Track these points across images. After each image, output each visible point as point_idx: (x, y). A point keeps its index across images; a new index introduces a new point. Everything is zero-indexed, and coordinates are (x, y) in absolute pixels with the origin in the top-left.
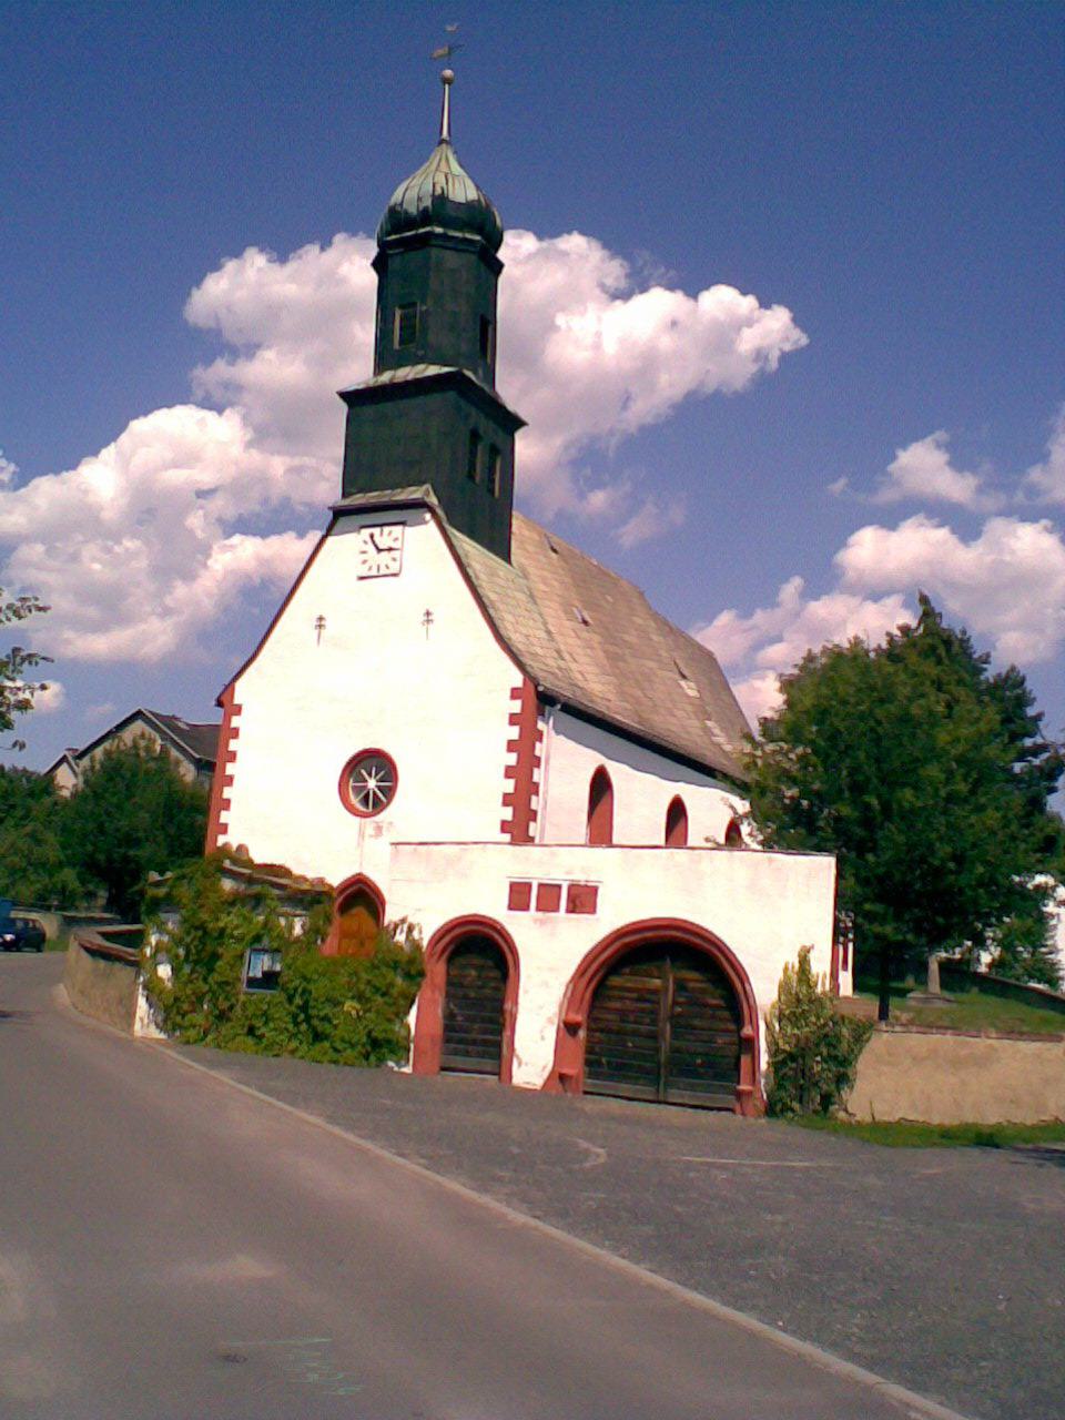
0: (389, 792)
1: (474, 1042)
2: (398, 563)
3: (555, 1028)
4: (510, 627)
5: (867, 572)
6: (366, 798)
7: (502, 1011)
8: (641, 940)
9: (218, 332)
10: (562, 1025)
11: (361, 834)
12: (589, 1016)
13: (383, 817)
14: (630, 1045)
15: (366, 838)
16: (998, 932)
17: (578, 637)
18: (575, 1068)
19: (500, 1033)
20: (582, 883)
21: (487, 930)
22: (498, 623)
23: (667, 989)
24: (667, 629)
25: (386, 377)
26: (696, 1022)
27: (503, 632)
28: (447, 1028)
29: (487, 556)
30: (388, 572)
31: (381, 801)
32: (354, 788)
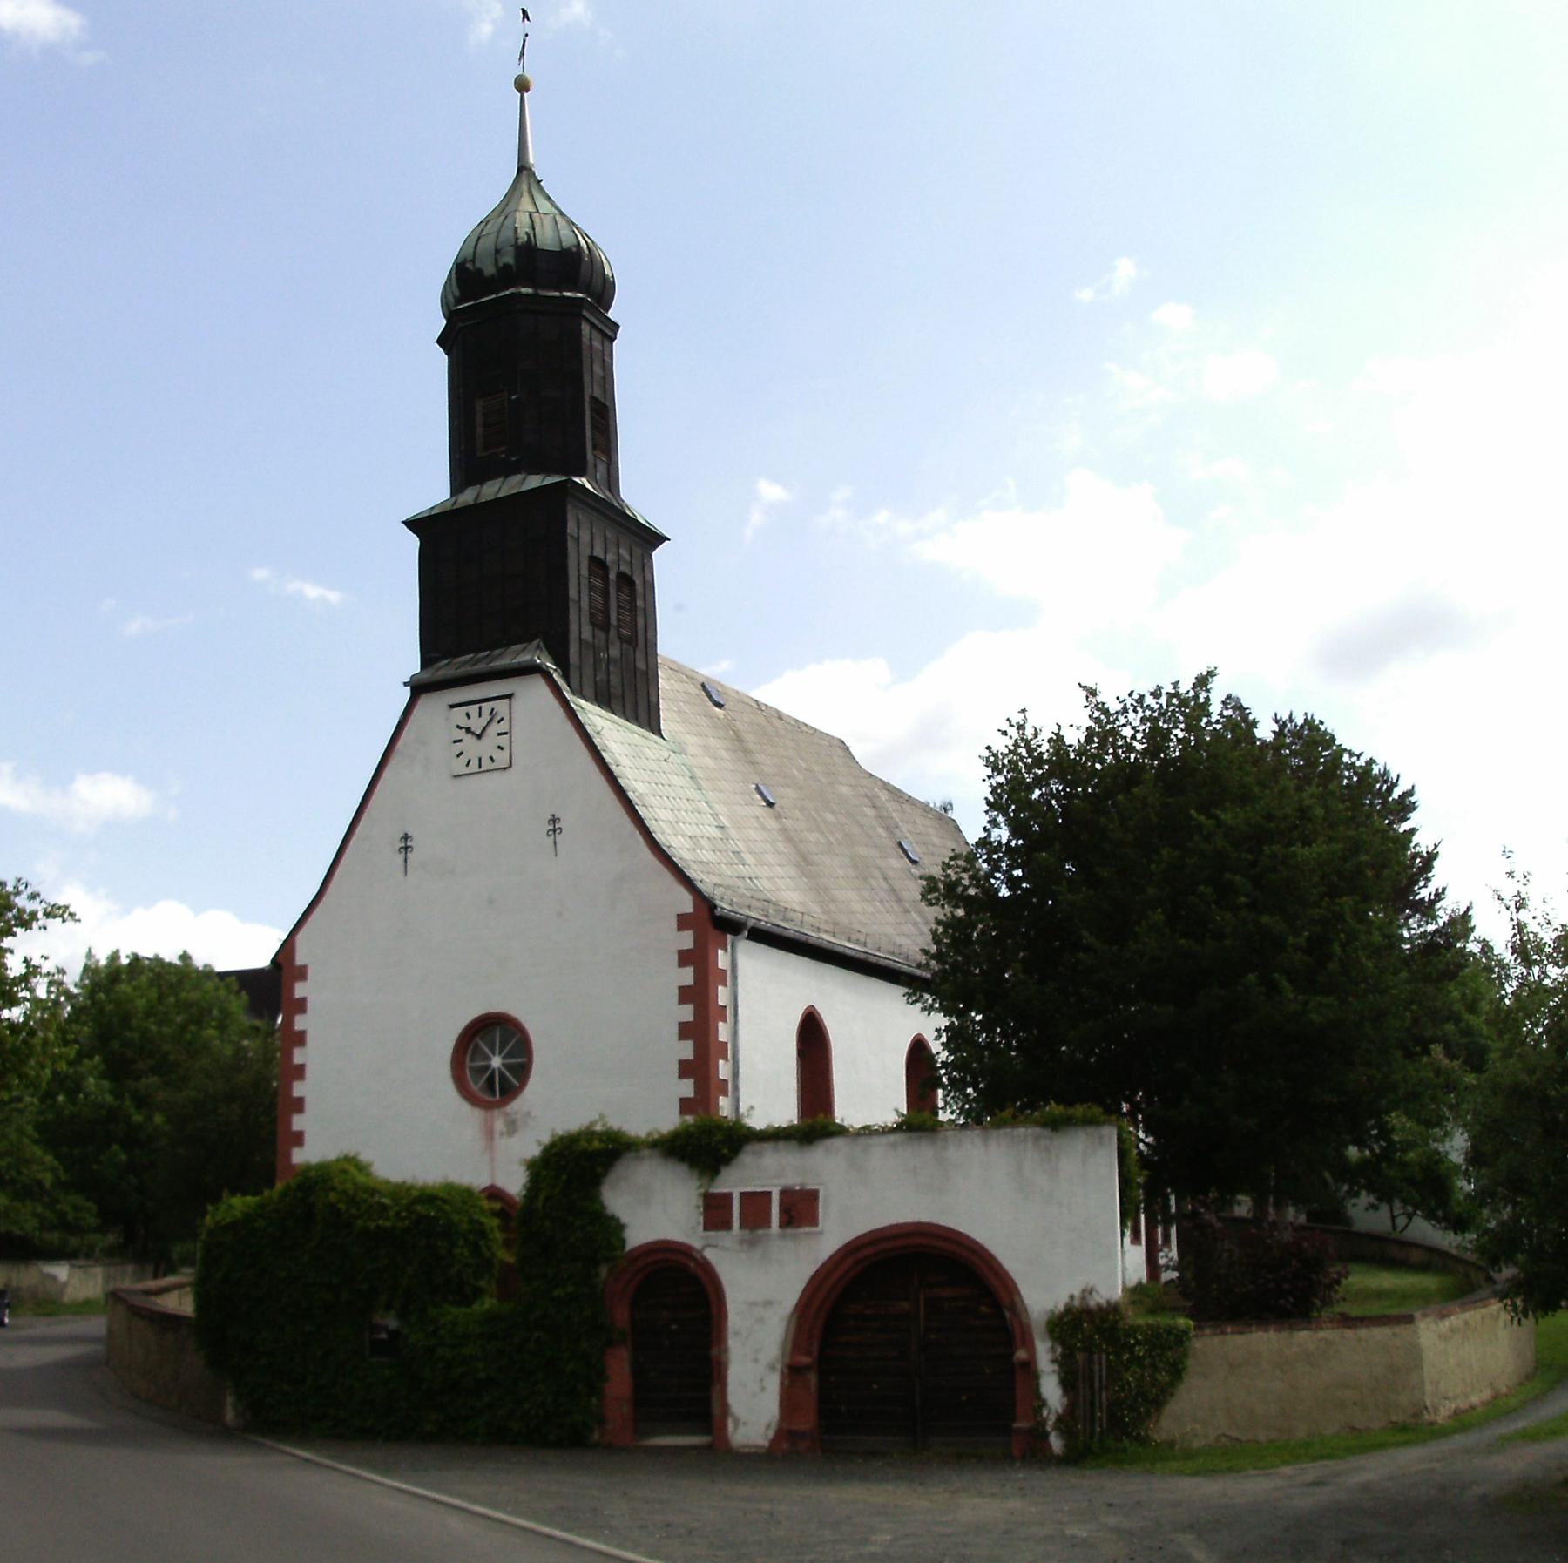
0: (522, 1071)
2: (506, 752)
4: (667, 829)
6: (490, 1082)
11: (489, 1134)
13: (516, 1105)
14: (875, 1386)
15: (497, 1136)
16: (1485, 1216)
17: (764, 828)
18: (806, 1422)
22: (651, 824)
25: (468, 497)
27: (658, 836)
29: (763, 1186)
30: (493, 766)
31: (512, 1085)
32: (472, 1069)
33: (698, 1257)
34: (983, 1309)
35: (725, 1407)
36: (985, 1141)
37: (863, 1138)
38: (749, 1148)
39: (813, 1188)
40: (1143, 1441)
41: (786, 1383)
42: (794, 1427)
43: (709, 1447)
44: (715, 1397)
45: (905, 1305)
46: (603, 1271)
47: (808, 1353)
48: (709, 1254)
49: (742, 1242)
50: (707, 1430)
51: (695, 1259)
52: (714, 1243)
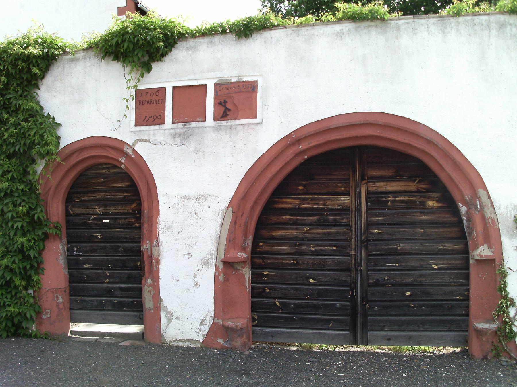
1: (109, 292)
3: (211, 272)
5: (38, 92)
7: (139, 253)
8: (329, 303)
9: (510, 14)
10: (221, 266)
12: (255, 252)
19: (139, 281)
20: (234, 80)
21: (112, 154)
23: (358, 210)
24: (242, 126)
26: (402, 246)
28: (72, 279)
33: (130, 151)
34: (431, 203)
35: (157, 299)
36: (443, 30)
37: (304, 29)
38: (181, 45)
39: (250, 79)
40: (223, 262)
41: (221, 278)
42: (230, 323)
43: (141, 336)
44: (147, 290)
45: (344, 200)
46: (40, 167)
47: (243, 249)
48: (140, 148)
49: (174, 136)
50: (139, 321)
51: (125, 154)
52: (146, 138)
